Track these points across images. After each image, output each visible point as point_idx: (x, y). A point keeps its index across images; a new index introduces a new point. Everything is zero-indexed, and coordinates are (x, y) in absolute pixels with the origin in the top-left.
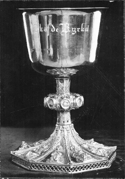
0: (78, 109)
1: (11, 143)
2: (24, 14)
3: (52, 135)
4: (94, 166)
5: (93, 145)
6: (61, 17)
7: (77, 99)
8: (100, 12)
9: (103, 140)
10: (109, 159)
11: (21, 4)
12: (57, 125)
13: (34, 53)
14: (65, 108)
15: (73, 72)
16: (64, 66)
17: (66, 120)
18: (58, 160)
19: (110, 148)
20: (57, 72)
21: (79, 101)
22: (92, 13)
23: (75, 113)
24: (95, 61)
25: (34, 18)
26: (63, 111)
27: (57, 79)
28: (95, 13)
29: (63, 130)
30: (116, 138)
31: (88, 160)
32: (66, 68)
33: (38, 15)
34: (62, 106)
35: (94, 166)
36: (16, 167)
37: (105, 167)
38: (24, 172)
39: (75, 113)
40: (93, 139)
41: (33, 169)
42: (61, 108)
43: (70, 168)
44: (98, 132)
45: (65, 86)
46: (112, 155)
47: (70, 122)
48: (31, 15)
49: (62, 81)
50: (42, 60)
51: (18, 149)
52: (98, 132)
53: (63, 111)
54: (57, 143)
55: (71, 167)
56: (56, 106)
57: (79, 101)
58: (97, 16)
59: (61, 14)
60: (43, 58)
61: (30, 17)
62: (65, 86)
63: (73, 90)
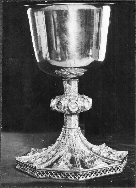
0: (53, 98)
1: (19, 149)
2: (29, 11)
3: (58, 139)
4: (94, 174)
5: (103, 149)
6: (66, 13)
7: (85, 101)
8: (109, 6)
9: (117, 145)
10: (122, 162)
11: (26, 3)
12: (63, 129)
13: (40, 54)
14: (74, 111)
15: (81, 72)
16: (73, 65)
17: (73, 122)
18: (63, 166)
19: (120, 152)
20: (64, 72)
21: (87, 103)
22: (100, 8)
23: (84, 117)
24: (105, 60)
25: (40, 17)
26: (71, 114)
27: (65, 80)
28: (104, 7)
29: (65, 133)
30: (131, 144)
31: (100, 165)
32: (75, 67)
33: (43, 12)
34: (71, 110)
35: (94, 174)
36: (24, 175)
37: (118, 172)
38: (33, 180)
39: (84, 117)
40: (104, 144)
41: (39, 175)
42: (69, 110)
43: (79, 174)
44: (111, 136)
45: (72, 87)
46: (124, 159)
47: (77, 126)
48: (37, 11)
49: (69, 82)
50: (49, 59)
51: (25, 155)
52: (111, 136)
53: (71, 114)
54: (64, 150)
55: (81, 173)
56: (64, 109)
57: (87, 103)
58: (107, 10)
59: (66, 9)
60: (51, 58)
61: (35, 14)
62: (72, 87)
63: (82, 91)
